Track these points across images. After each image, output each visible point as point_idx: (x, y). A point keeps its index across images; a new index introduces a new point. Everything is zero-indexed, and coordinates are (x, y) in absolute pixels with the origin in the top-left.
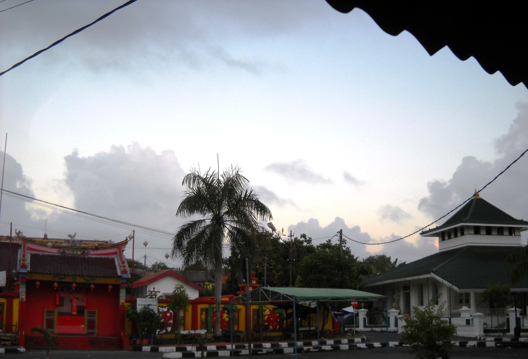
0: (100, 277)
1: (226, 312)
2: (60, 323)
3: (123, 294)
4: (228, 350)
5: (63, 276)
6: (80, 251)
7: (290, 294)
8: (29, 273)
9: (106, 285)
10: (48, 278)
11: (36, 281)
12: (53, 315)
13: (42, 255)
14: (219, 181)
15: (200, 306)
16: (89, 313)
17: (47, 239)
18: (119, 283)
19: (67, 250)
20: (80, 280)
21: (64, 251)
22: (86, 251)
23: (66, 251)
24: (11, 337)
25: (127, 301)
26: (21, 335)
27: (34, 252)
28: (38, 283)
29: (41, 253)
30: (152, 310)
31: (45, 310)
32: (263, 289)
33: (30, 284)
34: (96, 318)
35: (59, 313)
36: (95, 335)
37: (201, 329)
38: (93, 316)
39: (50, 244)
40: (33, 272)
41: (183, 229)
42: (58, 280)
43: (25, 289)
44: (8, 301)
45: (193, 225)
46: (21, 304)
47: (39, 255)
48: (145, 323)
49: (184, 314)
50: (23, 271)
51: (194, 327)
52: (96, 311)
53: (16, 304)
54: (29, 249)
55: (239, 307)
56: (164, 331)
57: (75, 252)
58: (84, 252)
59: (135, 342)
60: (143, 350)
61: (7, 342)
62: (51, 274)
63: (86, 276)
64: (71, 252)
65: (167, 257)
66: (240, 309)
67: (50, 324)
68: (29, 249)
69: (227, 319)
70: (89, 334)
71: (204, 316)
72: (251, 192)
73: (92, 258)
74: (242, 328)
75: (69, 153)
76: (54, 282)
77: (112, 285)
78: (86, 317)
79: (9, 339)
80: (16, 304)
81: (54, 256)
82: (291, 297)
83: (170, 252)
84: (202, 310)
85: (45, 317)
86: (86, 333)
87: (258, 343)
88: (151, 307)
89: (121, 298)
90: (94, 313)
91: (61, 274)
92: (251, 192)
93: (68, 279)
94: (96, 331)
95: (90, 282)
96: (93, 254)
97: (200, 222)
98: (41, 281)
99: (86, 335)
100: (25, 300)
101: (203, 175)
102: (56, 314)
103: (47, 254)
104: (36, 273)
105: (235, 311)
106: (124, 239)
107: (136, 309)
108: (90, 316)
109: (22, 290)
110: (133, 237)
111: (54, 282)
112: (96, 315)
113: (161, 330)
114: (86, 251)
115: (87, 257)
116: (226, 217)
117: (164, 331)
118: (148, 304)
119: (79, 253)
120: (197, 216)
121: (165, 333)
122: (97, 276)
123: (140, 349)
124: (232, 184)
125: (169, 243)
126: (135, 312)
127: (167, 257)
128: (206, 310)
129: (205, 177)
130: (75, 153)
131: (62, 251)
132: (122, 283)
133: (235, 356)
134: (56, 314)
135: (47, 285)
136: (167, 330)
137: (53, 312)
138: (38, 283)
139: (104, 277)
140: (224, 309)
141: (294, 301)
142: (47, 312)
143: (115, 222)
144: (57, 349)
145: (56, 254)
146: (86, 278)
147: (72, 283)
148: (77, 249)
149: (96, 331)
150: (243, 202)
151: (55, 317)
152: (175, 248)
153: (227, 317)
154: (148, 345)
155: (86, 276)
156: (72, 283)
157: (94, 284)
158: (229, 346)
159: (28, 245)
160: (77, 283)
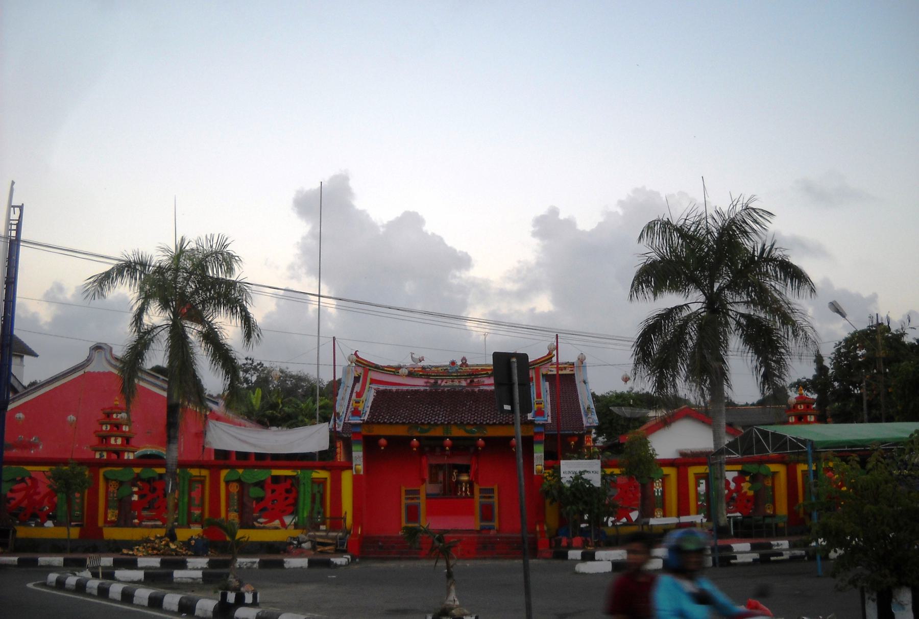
0: (494, 424)
1: (748, 478)
2: (430, 512)
3: (539, 452)
4: (141, 569)
5: (426, 427)
6: (466, 380)
7: (803, 437)
8: (366, 423)
9: (407, 440)
10: (401, 431)
11: (379, 437)
12: (419, 498)
13: (397, 391)
14: (709, 232)
15: (693, 471)
16: (481, 491)
17: (467, 366)
18: (531, 434)
19: (443, 380)
20: (457, 432)
21: (436, 382)
22: (476, 380)
23: (439, 382)
24: (335, 538)
25: (546, 468)
26: (355, 534)
27: (382, 387)
28: (383, 441)
29: (394, 388)
30: (588, 482)
31: (403, 489)
32: (758, 429)
33: (370, 444)
34: (495, 500)
35: (427, 495)
36: (492, 532)
37: (698, 513)
38: (490, 497)
39: (404, 371)
40: (373, 423)
41: (649, 326)
42: (418, 434)
43: (361, 454)
44: (211, 474)
45: (669, 314)
46: (356, 479)
47: (390, 391)
48: (574, 507)
49: (663, 487)
50: (356, 420)
51: (683, 510)
52: (496, 488)
53: (347, 479)
54: (373, 381)
55: (773, 468)
56: (624, 520)
57: (456, 383)
58: (472, 381)
59: (559, 542)
60: (569, 557)
61: (327, 548)
62: (403, 423)
63: (468, 424)
64: (450, 383)
65: (626, 380)
66: (667, 475)
67: (413, 514)
68: (373, 381)
69: (751, 493)
70: (483, 529)
71: (702, 488)
72: (772, 246)
73: (486, 391)
74: (782, 509)
75: (542, 210)
76: (411, 438)
77: (385, 437)
78: (478, 499)
79: (330, 541)
80: (347, 479)
81: (416, 392)
82: (804, 442)
83: (629, 370)
84: (698, 477)
85: (404, 502)
86: (478, 528)
87: (763, 541)
88: (585, 476)
89: (536, 462)
90: (492, 491)
91: (423, 424)
92: (772, 246)
93: (438, 432)
94: (495, 524)
95: (477, 435)
96: (445, 384)
97: (680, 308)
98: (389, 438)
99: (478, 532)
100: (362, 473)
101: (677, 220)
102: (423, 496)
103: (405, 388)
104: (379, 423)
105: (766, 476)
106: (545, 353)
107: (560, 478)
108: (485, 497)
109: (358, 454)
110: (557, 348)
111: (412, 438)
112: (496, 495)
113: (619, 519)
114: (476, 380)
115: (476, 389)
116: (729, 295)
117: (624, 520)
118: (582, 470)
119: (464, 383)
120: (670, 300)
121: (624, 524)
122: (488, 424)
123: (565, 556)
124: (731, 234)
125: (626, 355)
126: (561, 487)
127: (626, 380)
128: (706, 477)
129: (681, 223)
130: (554, 212)
131: (432, 381)
132: (536, 433)
133: (721, 566)
134: (423, 496)
135: (398, 444)
136: (629, 518)
137: (418, 492)
138: (383, 441)
139: (500, 424)
140: (742, 473)
141: (810, 451)
142: (407, 492)
143: (440, 319)
144: (417, 559)
145: (422, 388)
146: (468, 428)
147: (443, 438)
148: (460, 376)
149: (495, 524)
150: (757, 264)
151: (422, 502)
152: (637, 364)
153: (750, 489)
154: (577, 548)
155: (468, 424)
156: (443, 438)
157: (483, 438)
158: (143, 562)
159: (372, 375)
160: (451, 438)
